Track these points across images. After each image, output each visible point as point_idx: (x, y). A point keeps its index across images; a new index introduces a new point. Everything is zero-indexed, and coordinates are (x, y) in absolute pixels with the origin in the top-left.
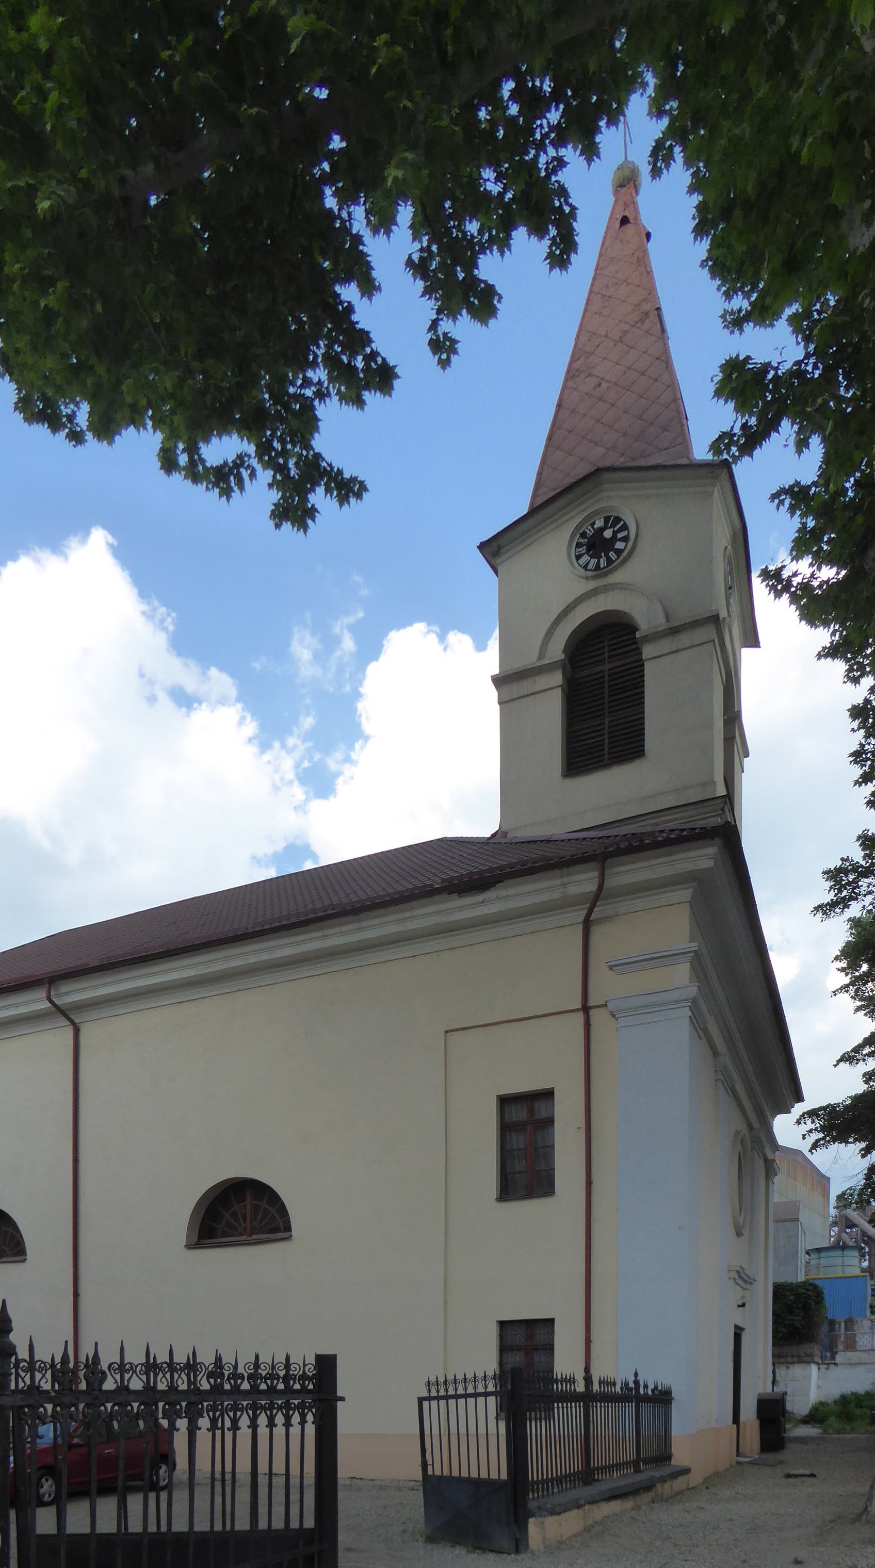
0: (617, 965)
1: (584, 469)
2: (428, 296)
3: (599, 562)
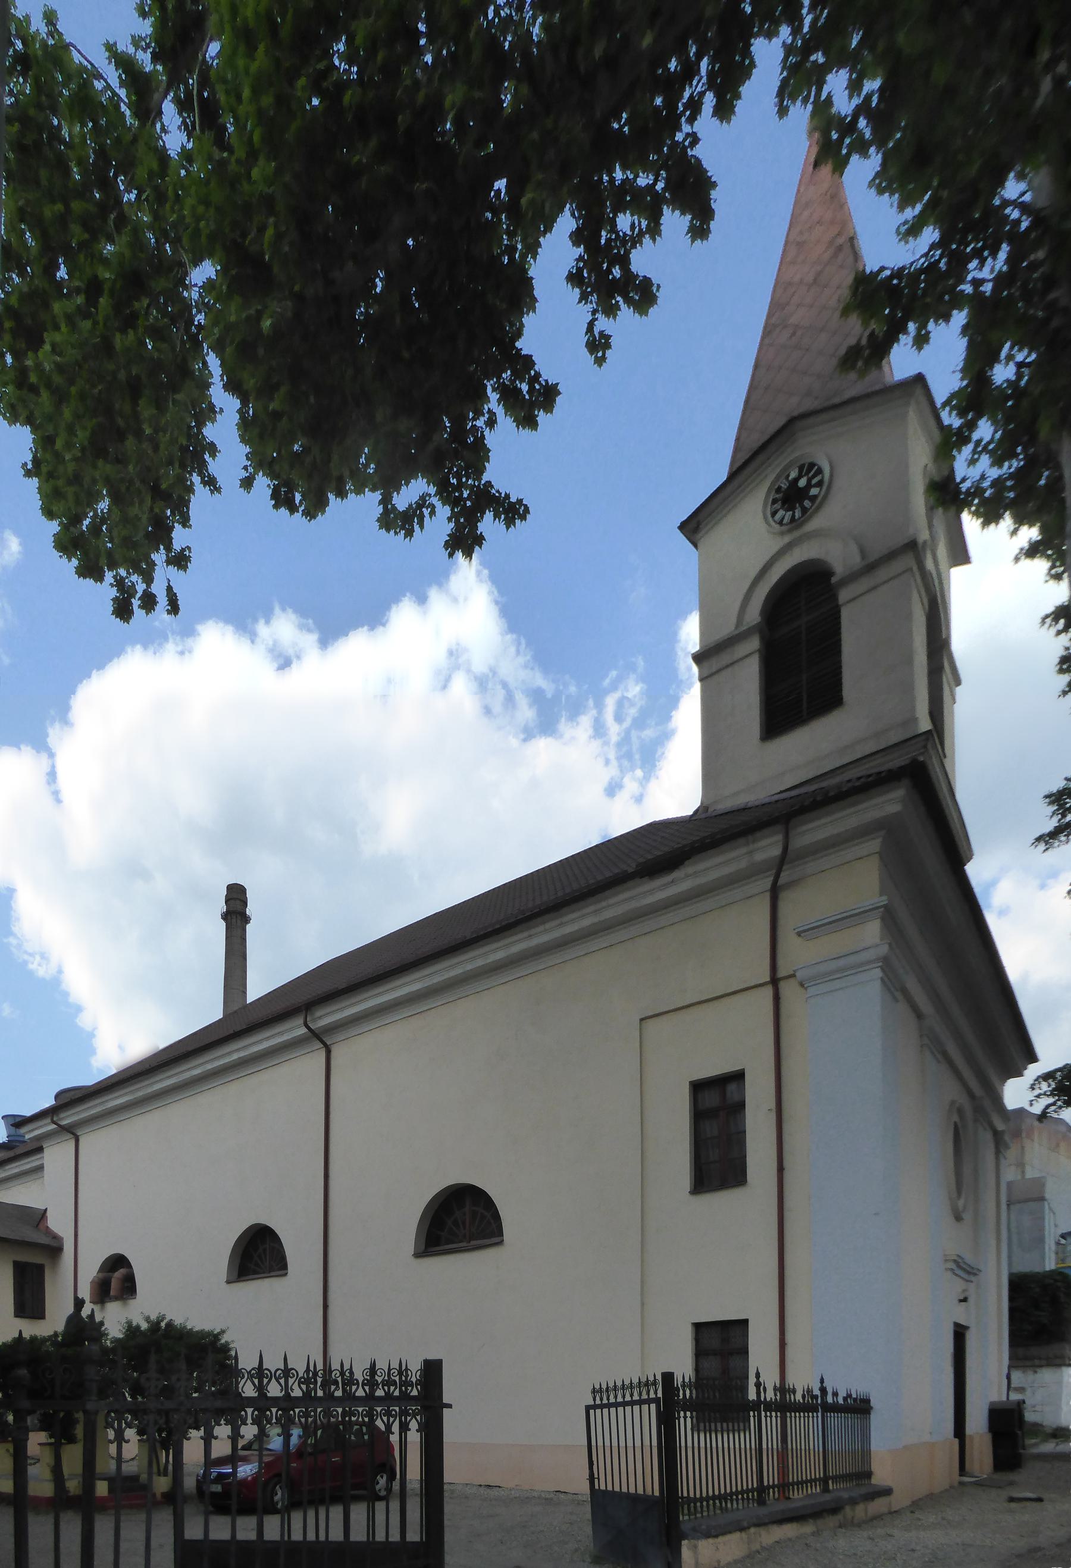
0: (805, 931)
1: (781, 421)
2: (584, 302)
3: (794, 513)
